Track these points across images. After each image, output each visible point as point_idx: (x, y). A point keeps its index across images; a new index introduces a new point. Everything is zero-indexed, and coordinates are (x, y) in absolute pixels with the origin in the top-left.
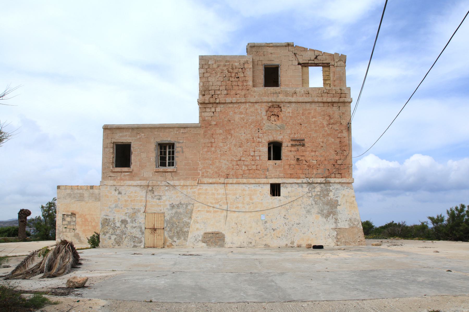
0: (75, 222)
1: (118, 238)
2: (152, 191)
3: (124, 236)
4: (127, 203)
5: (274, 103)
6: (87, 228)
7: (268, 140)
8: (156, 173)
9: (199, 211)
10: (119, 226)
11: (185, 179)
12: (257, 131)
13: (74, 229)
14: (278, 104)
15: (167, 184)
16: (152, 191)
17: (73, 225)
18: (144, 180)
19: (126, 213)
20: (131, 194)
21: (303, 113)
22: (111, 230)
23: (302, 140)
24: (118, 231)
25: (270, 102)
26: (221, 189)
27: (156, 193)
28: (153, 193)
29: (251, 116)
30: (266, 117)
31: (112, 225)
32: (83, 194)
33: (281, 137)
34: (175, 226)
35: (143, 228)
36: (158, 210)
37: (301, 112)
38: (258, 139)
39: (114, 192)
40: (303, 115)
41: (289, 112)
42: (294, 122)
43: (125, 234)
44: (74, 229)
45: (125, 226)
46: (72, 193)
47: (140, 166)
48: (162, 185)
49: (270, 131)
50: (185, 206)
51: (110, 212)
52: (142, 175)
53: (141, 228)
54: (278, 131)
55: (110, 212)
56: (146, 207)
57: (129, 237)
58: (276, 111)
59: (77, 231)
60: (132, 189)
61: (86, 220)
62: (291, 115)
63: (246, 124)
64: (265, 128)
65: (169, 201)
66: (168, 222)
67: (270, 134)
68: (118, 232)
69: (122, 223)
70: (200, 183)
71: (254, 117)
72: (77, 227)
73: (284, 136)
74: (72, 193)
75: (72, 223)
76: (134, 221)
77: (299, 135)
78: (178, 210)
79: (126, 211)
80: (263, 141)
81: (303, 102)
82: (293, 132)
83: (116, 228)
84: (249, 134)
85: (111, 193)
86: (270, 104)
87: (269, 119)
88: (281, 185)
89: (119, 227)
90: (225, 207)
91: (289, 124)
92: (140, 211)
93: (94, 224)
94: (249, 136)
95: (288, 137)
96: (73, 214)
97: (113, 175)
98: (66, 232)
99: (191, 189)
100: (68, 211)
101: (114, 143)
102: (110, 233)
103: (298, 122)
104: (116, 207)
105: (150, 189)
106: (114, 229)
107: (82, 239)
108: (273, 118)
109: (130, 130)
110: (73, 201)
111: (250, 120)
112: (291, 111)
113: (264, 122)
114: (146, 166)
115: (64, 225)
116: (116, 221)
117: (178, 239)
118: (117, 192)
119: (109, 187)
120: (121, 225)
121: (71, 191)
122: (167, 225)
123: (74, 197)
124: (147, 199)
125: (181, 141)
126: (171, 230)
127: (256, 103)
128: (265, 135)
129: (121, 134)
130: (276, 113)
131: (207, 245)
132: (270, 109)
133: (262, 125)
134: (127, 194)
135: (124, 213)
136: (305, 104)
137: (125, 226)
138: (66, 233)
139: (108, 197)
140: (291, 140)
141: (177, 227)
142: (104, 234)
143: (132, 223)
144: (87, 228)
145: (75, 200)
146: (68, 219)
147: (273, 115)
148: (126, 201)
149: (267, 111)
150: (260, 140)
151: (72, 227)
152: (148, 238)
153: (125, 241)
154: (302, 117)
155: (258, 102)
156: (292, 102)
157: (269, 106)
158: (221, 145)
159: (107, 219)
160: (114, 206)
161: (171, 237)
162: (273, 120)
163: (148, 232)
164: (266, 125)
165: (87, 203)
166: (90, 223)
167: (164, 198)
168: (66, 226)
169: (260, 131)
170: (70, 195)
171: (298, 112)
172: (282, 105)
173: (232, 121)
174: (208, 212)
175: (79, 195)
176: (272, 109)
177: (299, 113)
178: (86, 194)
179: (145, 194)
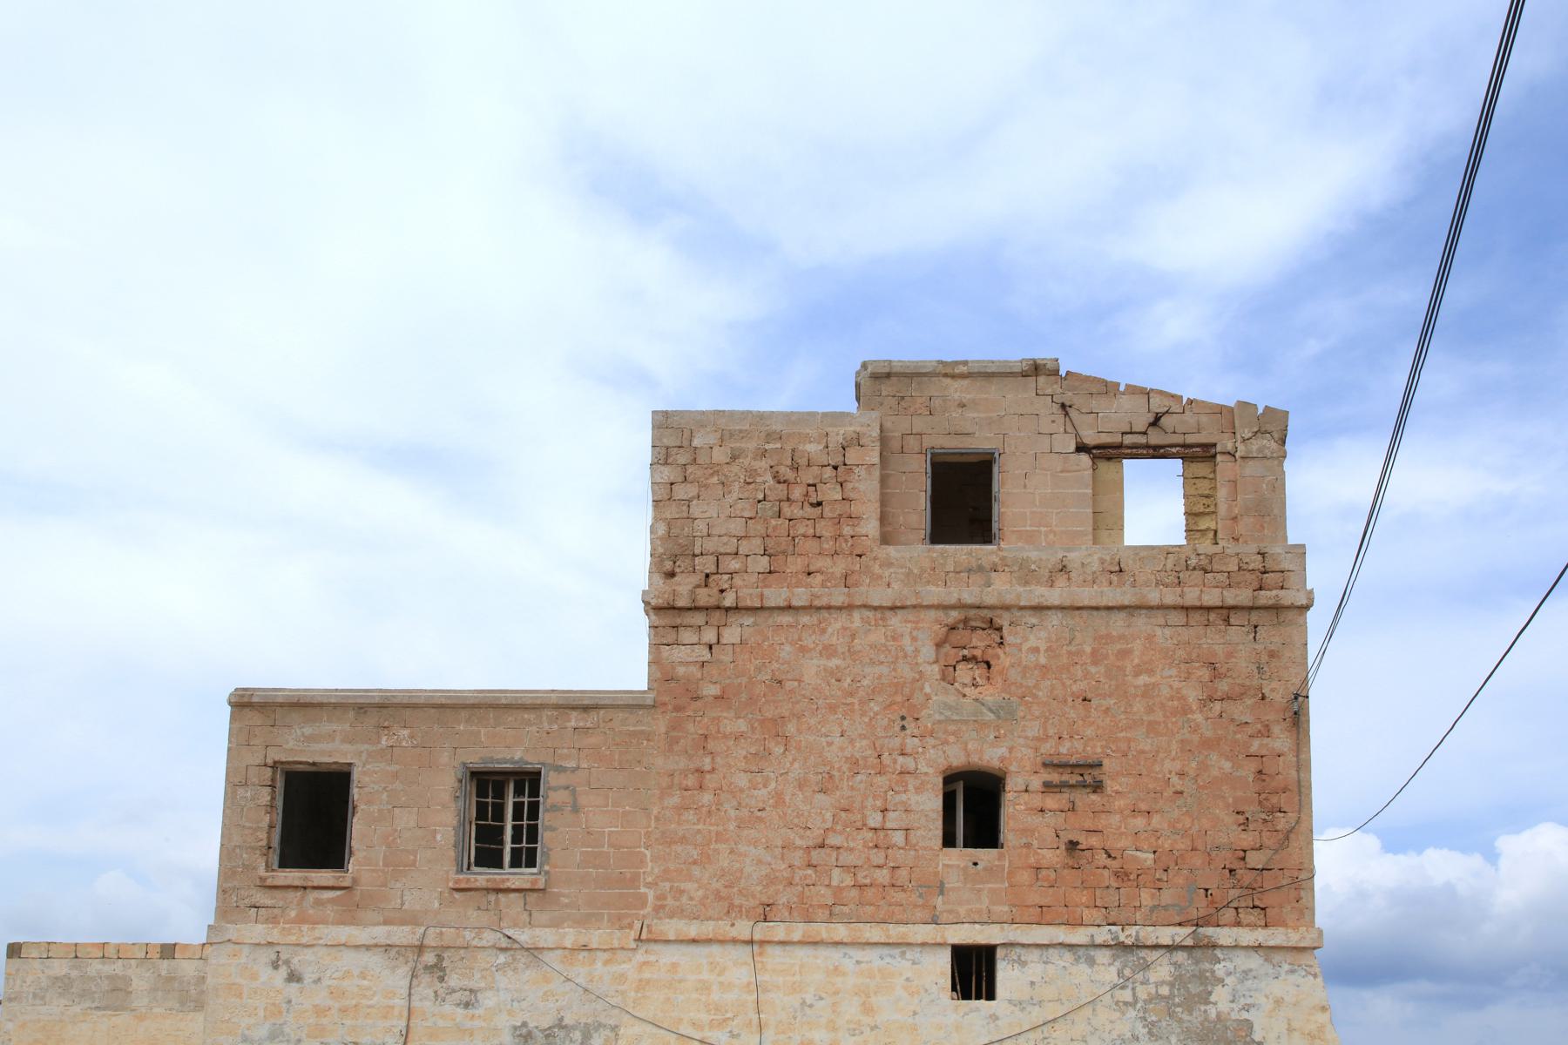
4: (325, 1021)
5: (972, 613)
7: (943, 764)
11: (583, 922)
12: (897, 728)
15: (504, 943)
20: (345, 983)
21: (1094, 652)
23: (1091, 766)
25: (953, 607)
26: (736, 966)
27: (453, 981)
28: (442, 979)
29: (872, 662)
30: (936, 668)
32: (127, 980)
33: (1002, 751)
37: (1088, 649)
38: (901, 759)
39: (266, 973)
40: (1095, 663)
41: (1036, 650)
42: (1059, 692)
46: (74, 974)
47: (386, 865)
48: (483, 943)
49: (952, 728)
58: (981, 644)
60: (350, 959)
62: (1043, 660)
63: (851, 695)
64: (931, 715)
67: (952, 739)
70: (649, 941)
71: (884, 670)
73: (1011, 749)
74: (74, 974)
77: (1079, 745)
80: (923, 768)
81: (1097, 608)
82: (1051, 732)
85: (254, 977)
86: (955, 615)
87: (948, 675)
88: (1000, 953)
91: (1035, 696)
94: (861, 748)
95: (1030, 753)
97: (269, 902)
101: (275, 765)
103: (1075, 688)
105: (430, 962)
108: (964, 673)
109: (351, 714)
110: (77, 1009)
111: (865, 682)
112: (1043, 647)
113: (927, 689)
114: (413, 864)
118: (283, 972)
119: (246, 950)
123: (83, 995)
127: (893, 608)
128: (931, 741)
130: (978, 653)
133: (918, 699)
134: (326, 982)
136: (1103, 613)
140: (1045, 765)
147: (965, 659)
148: (320, 1011)
149: (938, 645)
150: (909, 763)
154: (1093, 669)
155: (903, 608)
156: (1049, 608)
157: (950, 621)
158: (742, 780)
162: (968, 680)
164: (937, 700)
165: (141, 1018)
167: (488, 1000)
169: (911, 727)
170: (63, 985)
171: (1073, 648)
172: (1003, 620)
175: (105, 985)
176: (960, 636)
177: (1079, 653)
178: (141, 980)
179: (405, 983)
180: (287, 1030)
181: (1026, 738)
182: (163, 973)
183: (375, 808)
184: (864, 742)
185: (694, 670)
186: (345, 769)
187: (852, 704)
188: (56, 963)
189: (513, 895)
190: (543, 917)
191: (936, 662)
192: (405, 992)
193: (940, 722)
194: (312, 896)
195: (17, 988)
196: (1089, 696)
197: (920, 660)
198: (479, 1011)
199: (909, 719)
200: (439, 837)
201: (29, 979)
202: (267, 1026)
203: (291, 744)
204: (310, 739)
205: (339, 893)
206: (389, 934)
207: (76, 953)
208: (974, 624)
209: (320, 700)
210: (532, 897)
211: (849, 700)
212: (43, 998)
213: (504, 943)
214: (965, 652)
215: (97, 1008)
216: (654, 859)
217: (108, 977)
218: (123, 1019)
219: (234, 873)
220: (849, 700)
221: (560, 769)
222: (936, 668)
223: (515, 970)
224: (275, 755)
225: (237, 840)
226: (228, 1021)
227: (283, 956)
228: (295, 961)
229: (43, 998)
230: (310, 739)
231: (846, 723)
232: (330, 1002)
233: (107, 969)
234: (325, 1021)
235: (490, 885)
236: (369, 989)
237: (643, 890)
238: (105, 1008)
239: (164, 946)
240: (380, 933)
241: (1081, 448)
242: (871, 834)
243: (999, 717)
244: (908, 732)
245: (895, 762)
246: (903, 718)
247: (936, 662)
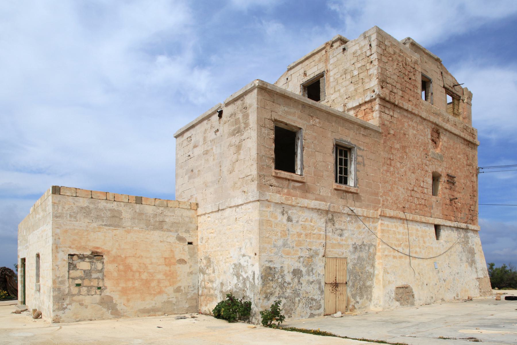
0: (101, 271)
1: (288, 304)
2: (332, 220)
3: (297, 299)
4: (301, 239)
6: (130, 284)
8: (336, 192)
9: (386, 255)
10: (290, 281)
11: (367, 207)
13: (99, 288)
14: (438, 128)
15: (350, 213)
16: (332, 220)
17: (98, 278)
18: (321, 200)
19: (299, 258)
20: (306, 223)
22: (278, 289)
24: (288, 291)
26: (400, 228)
27: (337, 226)
28: (333, 225)
31: (280, 280)
32: (120, 213)
34: (358, 278)
35: (323, 284)
36: (340, 253)
39: (280, 217)
43: (298, 295)
44: (99, 288)
45: (299, 281)
46: (92, 206)
47: (315, 175)
48: (345, 212)
50: (367, 248)
51: (276, 254)
52: (318, 192)
53: (320, 283)
55: (276, 254)
56: (325, 246)
57: (304, 301)
59: (107, 293)
60: (307, 214)
61: (128, 268)
65: (351, 239)
66: (351, 273)
68: (289, 292)
69: (295, 275)
70: (383, 216)
72: (108, 283)
74: (92, 206)
75: (94, 275)
76: (310, 271)
78: (361, 255)
79: (300, 254)
83: (286, 285)
85: (276, 218)
88: (441, 227)
89: (289, 284)
90: (407, 251)
92: (318, 255)
93: (144, 276)
96: (96, 255)
97: (277, 184)
98: (79, 294)
99: (373, 222)
100: (85, 248)
101: (276, 121)
102: (277, 294)
104: (284, 245)
105: (330, 216)
106: (282, 286)
107: (119, 308)
109: (300, 106)
110: (95, 225)
114: (322, 177)
115: (74, 279)
116: (286, 272)
117: (360, 299)
118: (286, 217)
119: (272, 205)
120: (292, 279)
121: (90, 203)
122: (350, 278)
123: (98, 217)
124: (328, 234)
125: (362, 148)
126: (353, 286)
129: (286, 109)
131: (401, 304)
134: (301, 223)
135: (297, 256)
137: (299, 281)
138: (81, 297)
139: (271, 226)
141: (360, 280)
142: (266, 297)
143: (309, 275)
144: (130, 284)
145: (101, 223)
146: (85, 265)
148: (299, 235)
151: (95, 283)
152: (329, 299)
153: (298, 309)
158: (398, 165)
159: (270, 268)
160: (280, 243)
161: (354, 296)
163: (328, 290)
165: (128, 232)
166: (137, 274)
167: (346, 234)
168: (78, 281)
170: (86, 211)
172: (441, 131)
173: (407, 136)
174: (394, 257)
175: (109, 214)
178: (127, 213)
179: (324, 225)
180: (289, 242)
182: (137, 211)
183: (310, 150)
185: (388, 123)
186: (295, 130)
188: (81, 200)
189: (350, 194)
190: (357, 204)
192: (324, 229)
194: (292, 184)
195: (60, 211)
198: (344, 238)
200: (329, 167)
201: (67, 207)
202: (282, 240)
203: (280, 113)
204: (287, 113)
205: (301, 184)
206: (320, 205)
207: (91, 195)
209: (291, 96)
210: (355, 195)
212: (75, 217)
213: (350, 213)
215: (105, 225)
216: (382, 187)
217: (110, 210)
218: (119, 232)
219: (263, 168)
221: (360, 149)
223: (352, 223)
224: (275, 116)
225: (263, 153)
226: (268, 237)
227: (286, 210)
228: (290, 212)
229: (75, 217)
230: (287, 113)
232: (302, 231)
233: (109, 205)
234: (301, 239)
235: (346, 190)
236: (313, 227)
237: (380, 198)
238: (110, 225)
239: (136, 197)
240: (314, 204)
241: (444, 87)
242: (421, 189)
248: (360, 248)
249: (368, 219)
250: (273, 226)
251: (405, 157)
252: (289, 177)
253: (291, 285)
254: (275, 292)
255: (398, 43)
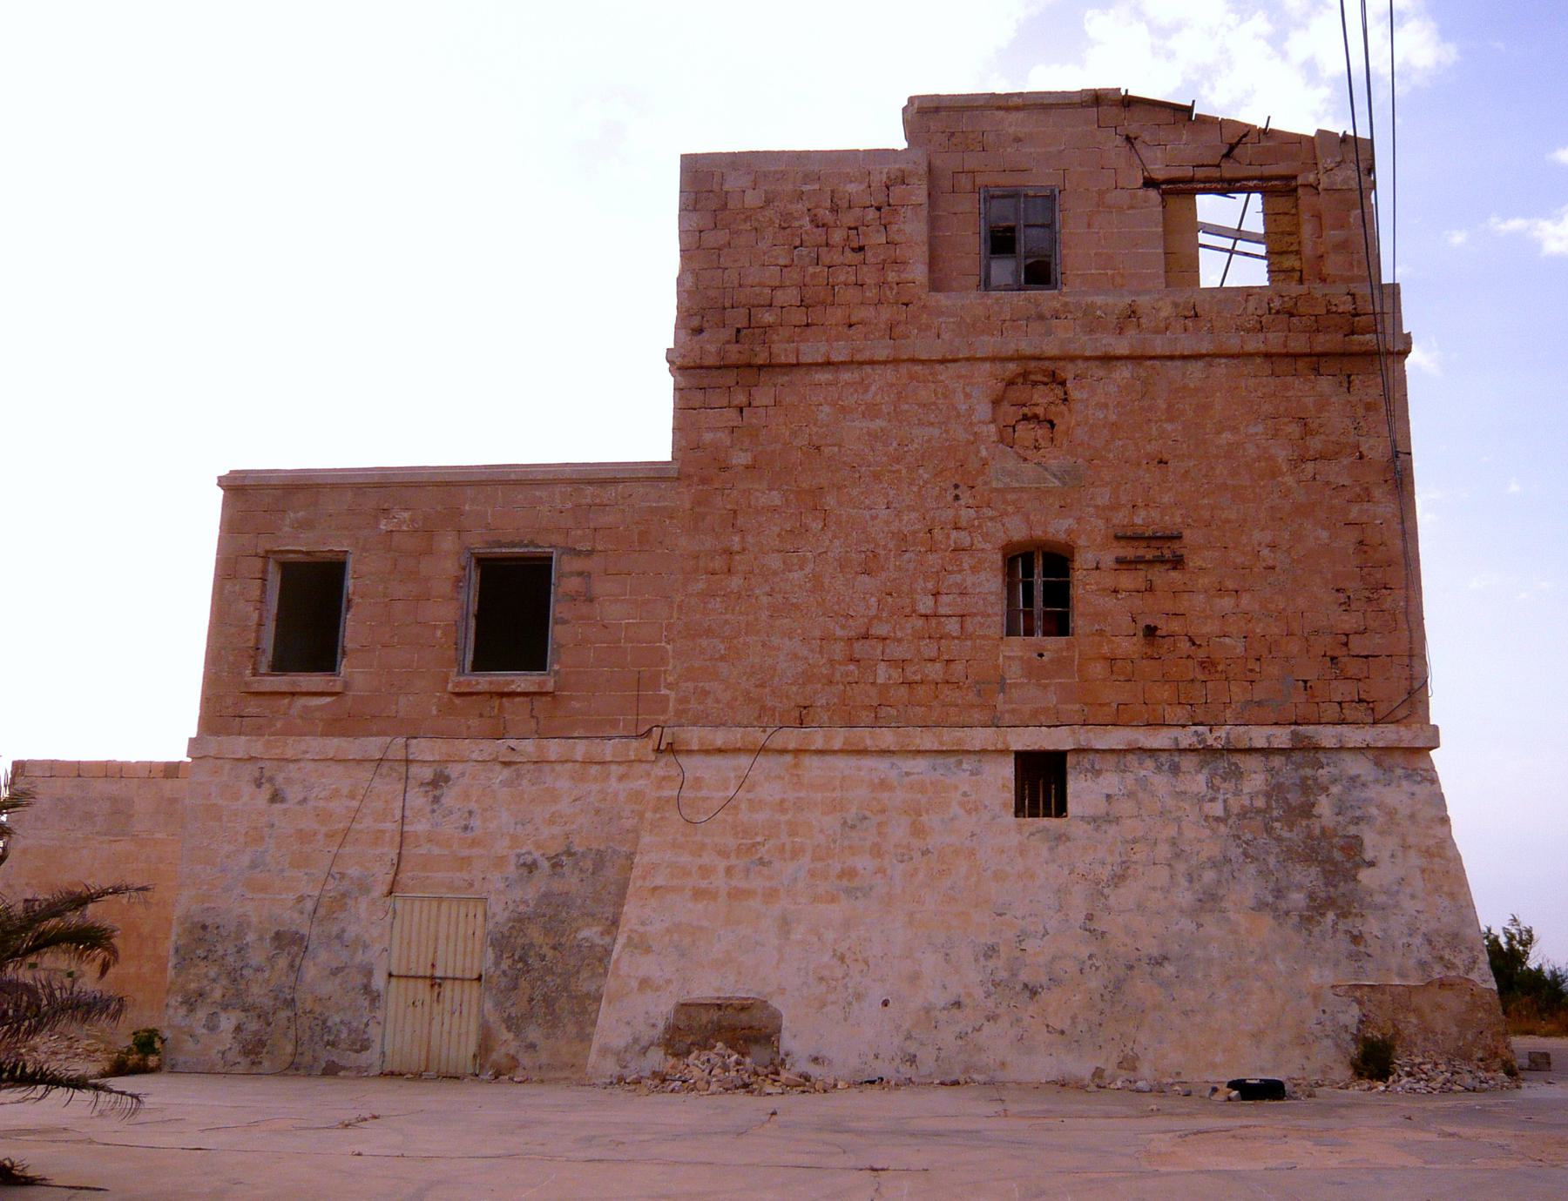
7: (1001, 538)
9: (655, 889)
12: (950, 498)
21: (1170, 406)
29: (921, 424)
30: (992, 428)
38: (954, 534)
39: (247, 789)
40: (1171, 420)
49: (1010, 497)
54: (1049, 491)
63: (898, 460)
67: (1010, 509)
69: (280, 947)
77: (1156, 514)
84: (911, 508)
87: (1006, 437)
88: (1070, 760)
108: (1025, 432)
118: (267, 791)
120: (271, 959)
130: (1040, 411)
132: (1014, 394)
133: (974, 464)
136: (1179, 363)
147: (1025, 418)
149: (996, 403)
150: (964, 538)
154: (1169, 427)
172: (1069, 371)
176: (1017, 393)
181: (1097, 507)
184: (914, 515)
187: (899, 471)
191: (994, 421)
193: (997, 490)
196: (1165, 458)
197: (975, 419)
199: (963, 488)
205: (329, 699)
208: (1033, 377)
210: (539, 703)
211: (896, 467)
214: (1025, 410)
220: (896, 467)
222: (992, 428)
227: (267, 774)
228: (280, 778)
231: (892, 493)
235: (494, 689)
237: (664, 692)
243: (1064, 484)
244: (962, 502)
245: (948, 537)
246: (956, 487)
247: (994, 421)
248: (554, 866)
249: (594, 769)
250: (225, 819)
251: (816, 526)
252: (284, 689)
253: (266, 975)
254: (212, 990)
255: (171, 770)
